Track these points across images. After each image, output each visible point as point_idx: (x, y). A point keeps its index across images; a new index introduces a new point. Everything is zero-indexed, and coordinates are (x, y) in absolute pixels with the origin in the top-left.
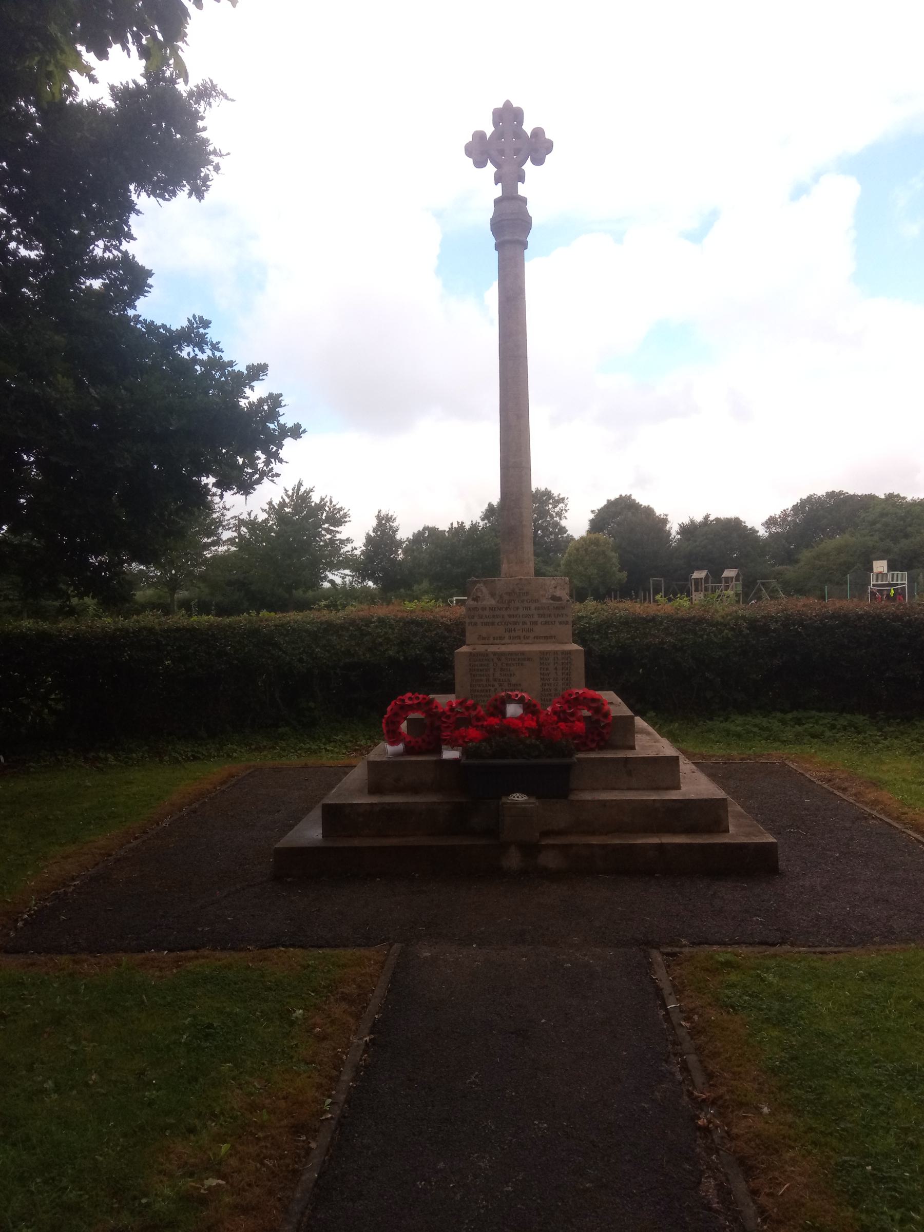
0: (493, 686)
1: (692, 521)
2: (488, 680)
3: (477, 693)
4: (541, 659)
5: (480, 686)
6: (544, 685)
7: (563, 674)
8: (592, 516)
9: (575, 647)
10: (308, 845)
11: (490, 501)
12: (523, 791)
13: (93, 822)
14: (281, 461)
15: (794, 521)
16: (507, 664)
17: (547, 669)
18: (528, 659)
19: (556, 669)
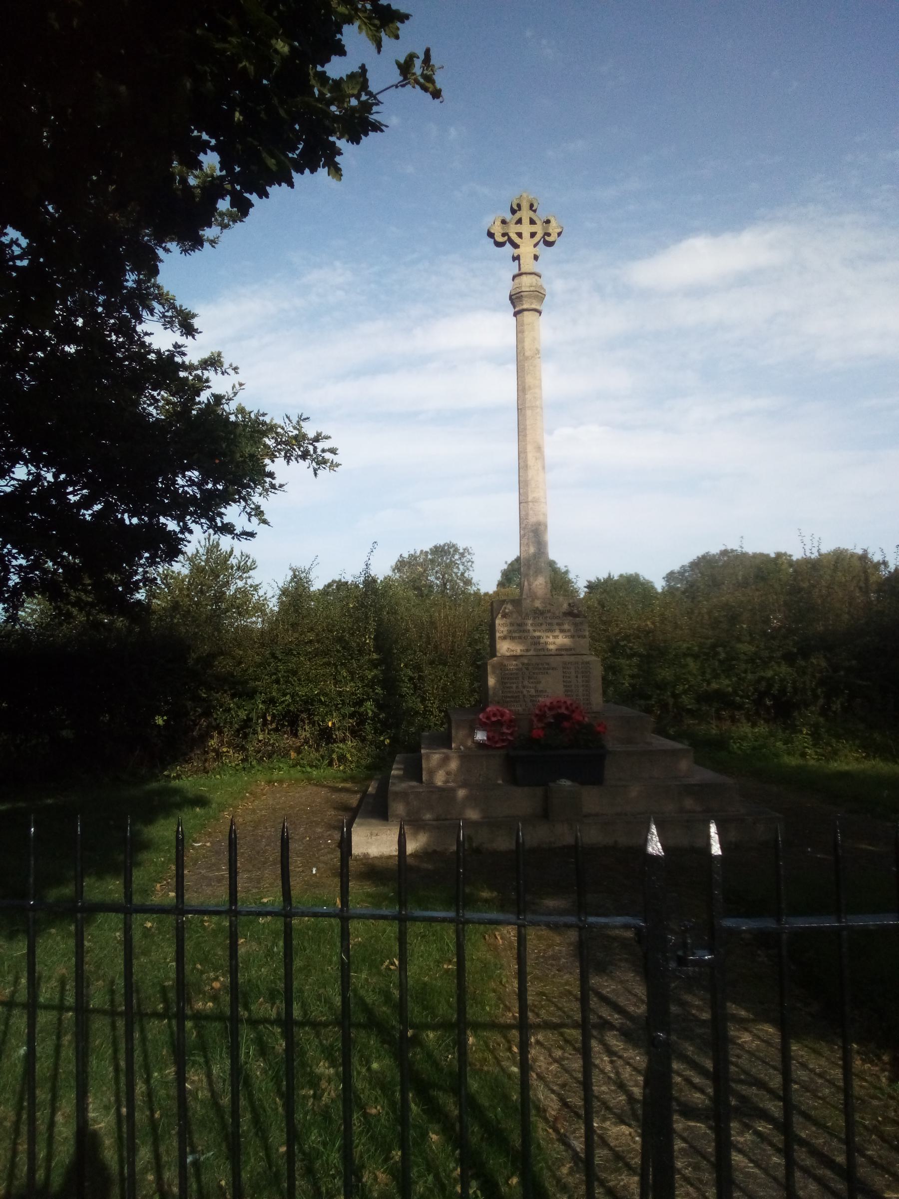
0: (522, 692)
1: (698, 557)
2: (517, 687)
3: (508, 699)
4: (564, 668)
5: (510, 692)
6: (566, 691)
7: (583, 681)
8: (506, 567)
9: (593, 658)
10: (374, 821)
11: (302, 563)
12: (568, 778)
13: (300, 756)
14: (415, 553)
15: (262, 628)
16: (534, 673)
17: (569, 677)
18: (553, 669)
19: (577, 677)
